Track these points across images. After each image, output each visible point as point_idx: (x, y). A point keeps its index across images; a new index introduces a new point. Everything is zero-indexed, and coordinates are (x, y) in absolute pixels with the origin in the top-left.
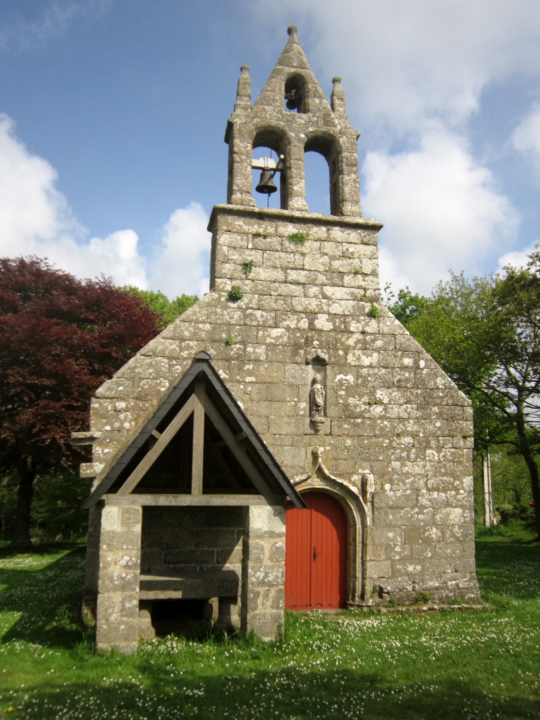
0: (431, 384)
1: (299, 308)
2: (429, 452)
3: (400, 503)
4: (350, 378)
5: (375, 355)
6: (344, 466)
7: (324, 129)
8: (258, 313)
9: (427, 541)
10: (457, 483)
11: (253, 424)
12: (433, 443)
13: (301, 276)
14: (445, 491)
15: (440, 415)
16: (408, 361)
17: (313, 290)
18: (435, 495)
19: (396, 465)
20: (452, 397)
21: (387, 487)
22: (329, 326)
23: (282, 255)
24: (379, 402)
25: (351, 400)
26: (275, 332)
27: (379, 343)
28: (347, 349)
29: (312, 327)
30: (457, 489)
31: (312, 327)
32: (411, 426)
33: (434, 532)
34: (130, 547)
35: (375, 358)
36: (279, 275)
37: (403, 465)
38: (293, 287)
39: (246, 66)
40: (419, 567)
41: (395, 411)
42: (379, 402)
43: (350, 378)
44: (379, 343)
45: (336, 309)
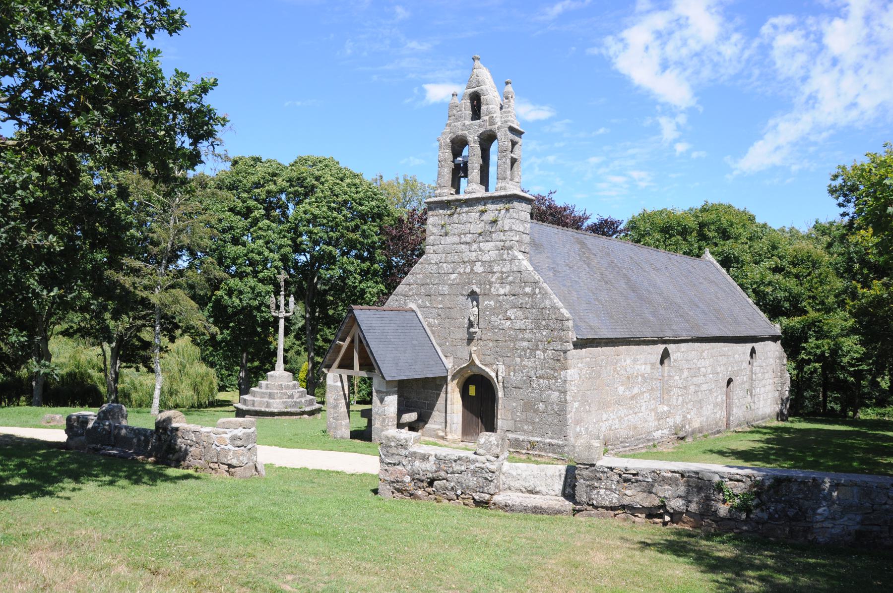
0: (542, 305)
1: (466, 259)
2: (538, 352)
3: (519, 385)
4: (492, 303)
5: (508, 286)
6: (489, 359)
7: (489, 128)
8: (445, 265)
9: (536, 411)
10: (556, 374)
11: (683, 345)
12: (541, 347)
13: (469, 238)
14: (548, 379)
15: (547, 327)
16: (528, 290)
17: (475, 246)
18: (541, 381)
19: (518, 360)
20: (555, 314)
21: (512, 374)
22: (482, 269)
23: (459, 226)
24: (509, 319)
25: (493, 318)
26: (453, 276)
27: (511, 278)
28: (491, 284)
29: (472, 271)
30: (556, 379)
31: (472, 271)
32: (527, 335)
33: (541, 406)
34: (7, 181)
35: (507, 289)
36: (456, 239)
37: (522, 360)
38: (463, 246)
39: (478, 56)
40: (531, 427)
41: (520, 324)
42: (509, 319)
43: (492, 303)
44: (511, 278)
45: (486, 258)
